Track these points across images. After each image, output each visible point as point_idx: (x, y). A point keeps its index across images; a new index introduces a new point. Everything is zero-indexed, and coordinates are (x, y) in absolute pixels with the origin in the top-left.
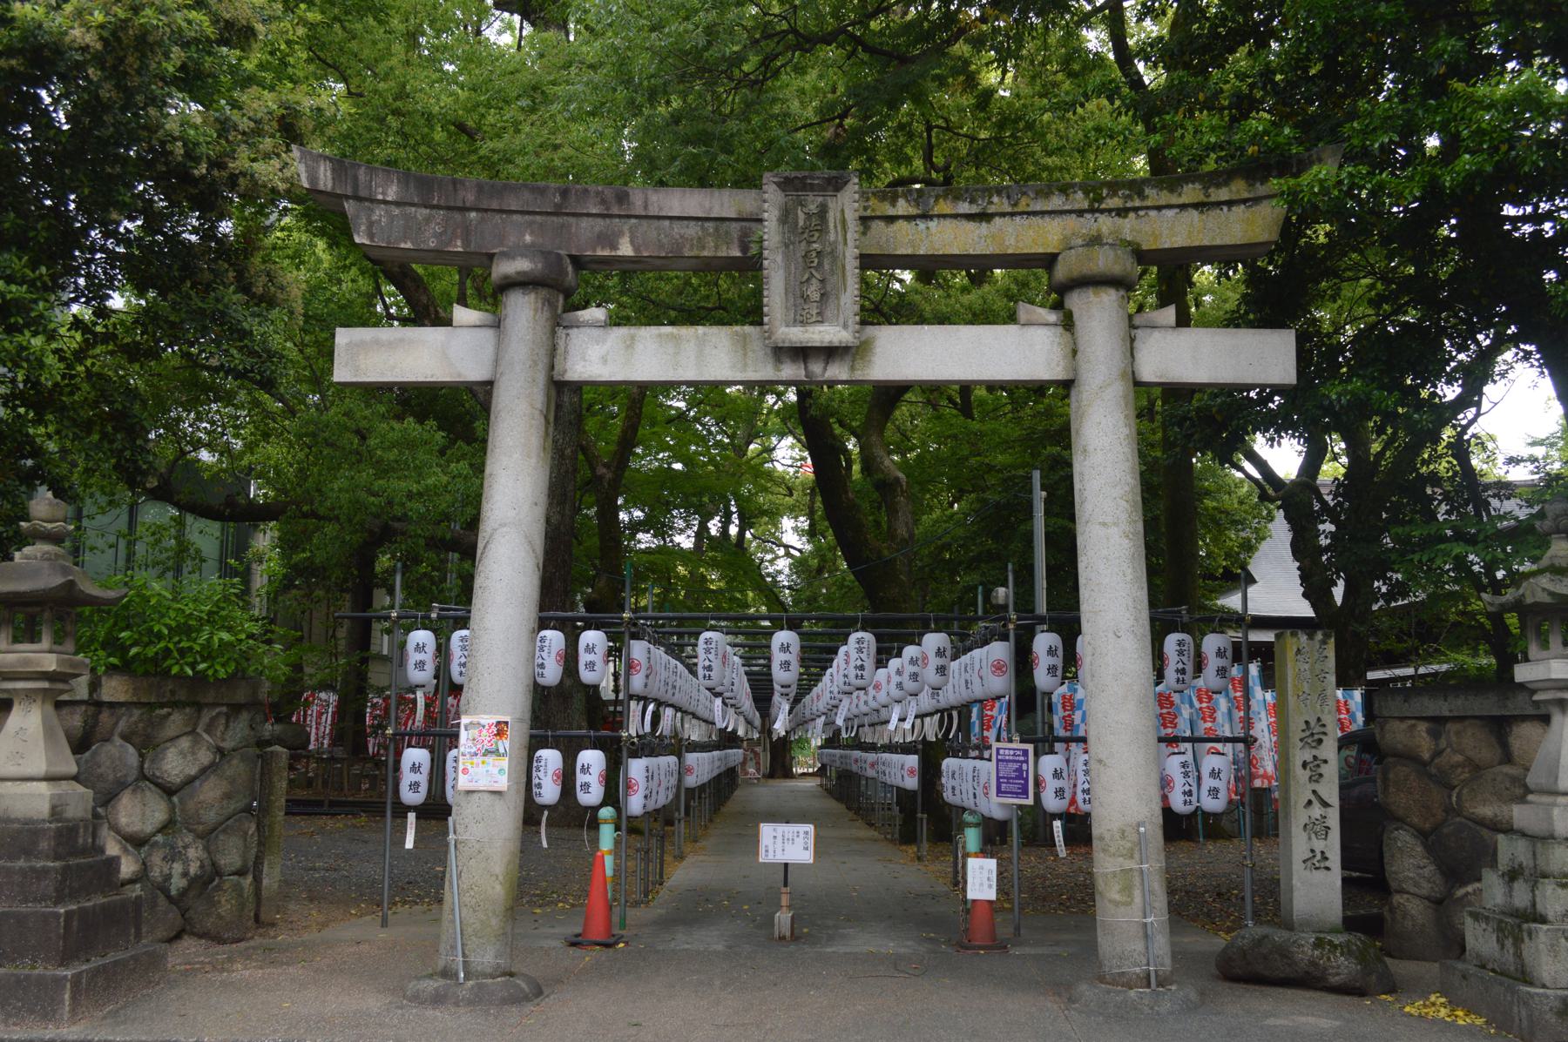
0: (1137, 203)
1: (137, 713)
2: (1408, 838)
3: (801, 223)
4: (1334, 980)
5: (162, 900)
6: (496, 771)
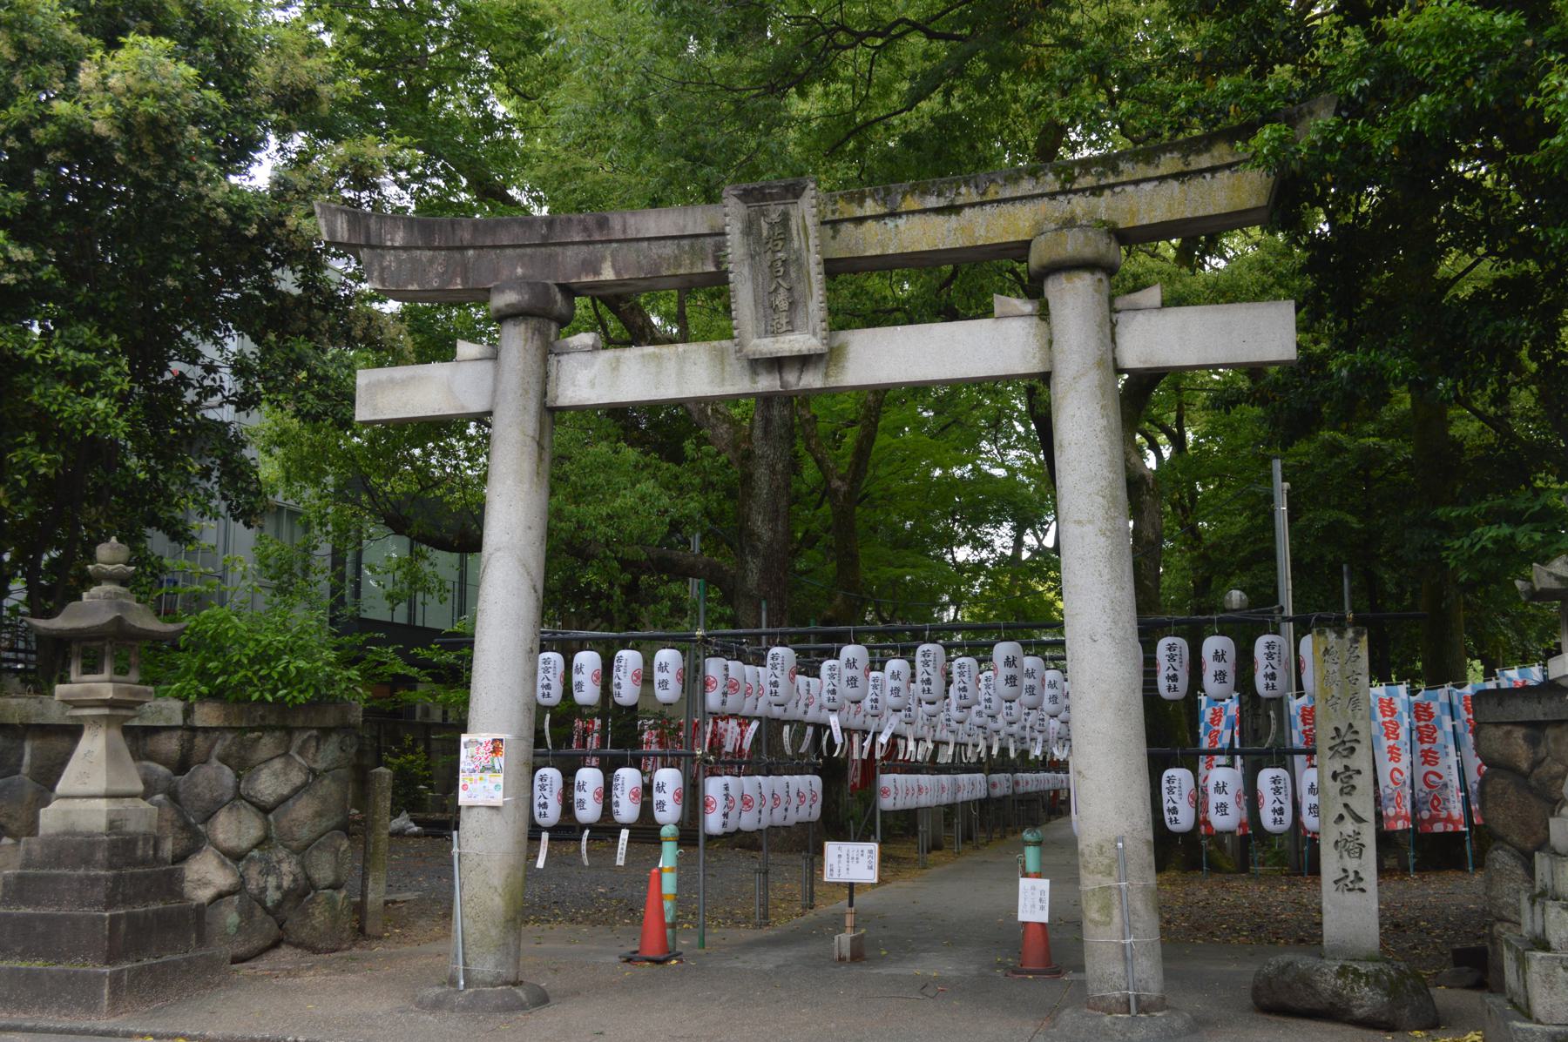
0: (1112, 180)
1: (230, 736)
2: (1507, 859)
3: (765, 233)
4: (1359, 1013)
5: (259, 912)
6: (492, 787)
